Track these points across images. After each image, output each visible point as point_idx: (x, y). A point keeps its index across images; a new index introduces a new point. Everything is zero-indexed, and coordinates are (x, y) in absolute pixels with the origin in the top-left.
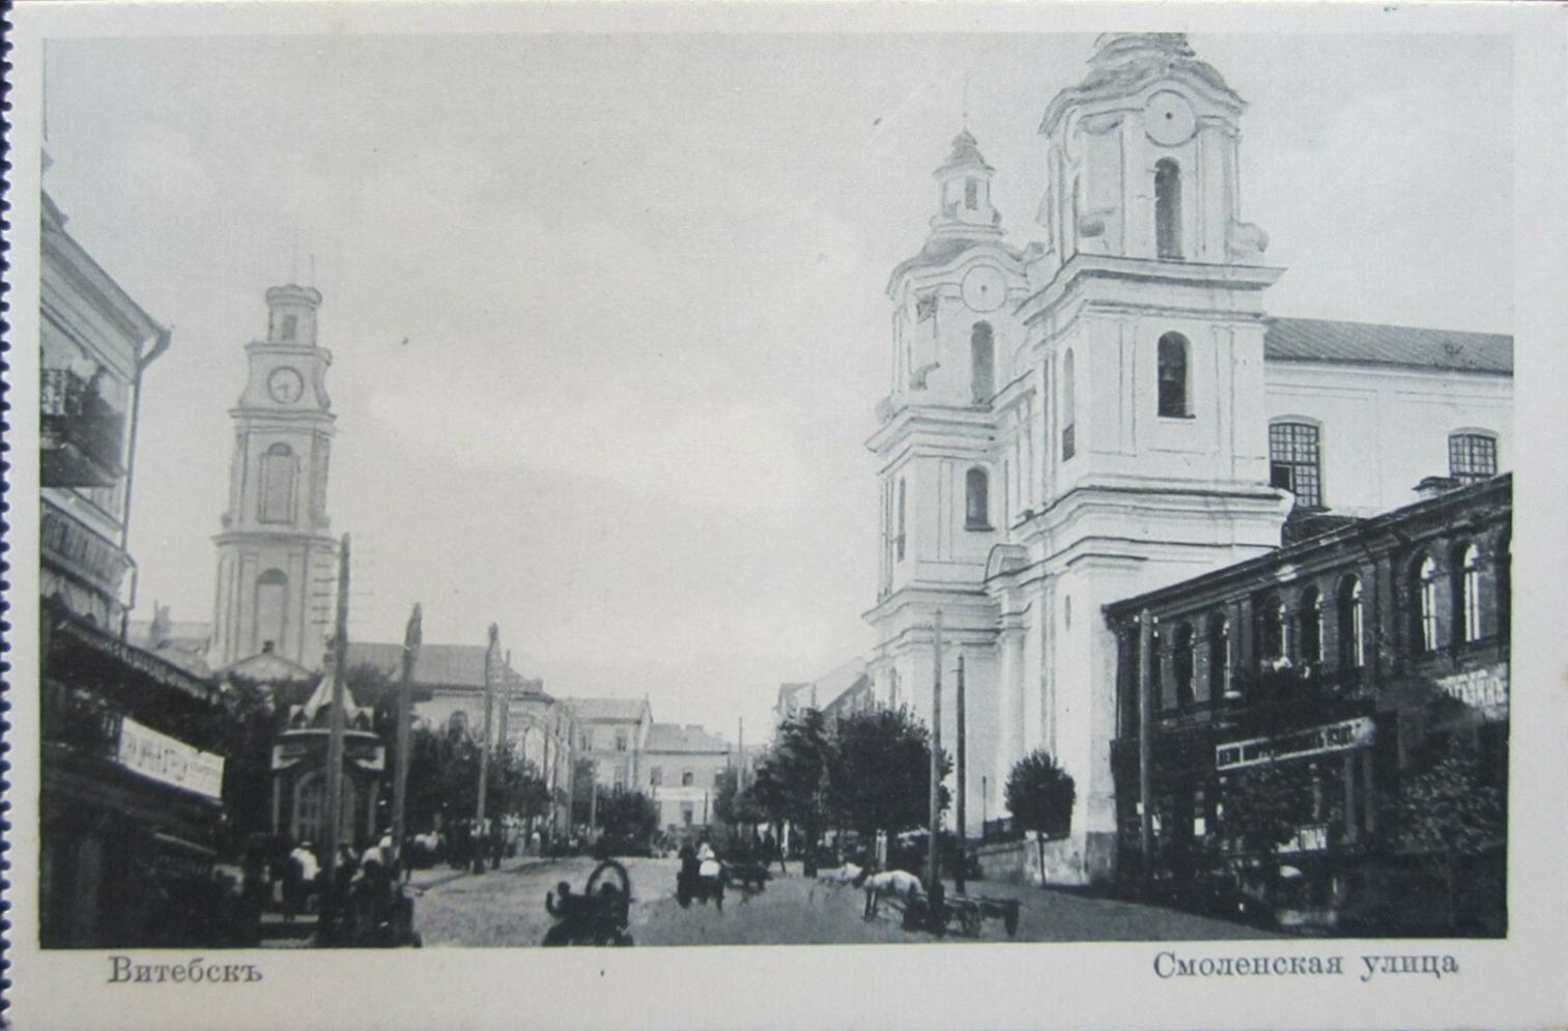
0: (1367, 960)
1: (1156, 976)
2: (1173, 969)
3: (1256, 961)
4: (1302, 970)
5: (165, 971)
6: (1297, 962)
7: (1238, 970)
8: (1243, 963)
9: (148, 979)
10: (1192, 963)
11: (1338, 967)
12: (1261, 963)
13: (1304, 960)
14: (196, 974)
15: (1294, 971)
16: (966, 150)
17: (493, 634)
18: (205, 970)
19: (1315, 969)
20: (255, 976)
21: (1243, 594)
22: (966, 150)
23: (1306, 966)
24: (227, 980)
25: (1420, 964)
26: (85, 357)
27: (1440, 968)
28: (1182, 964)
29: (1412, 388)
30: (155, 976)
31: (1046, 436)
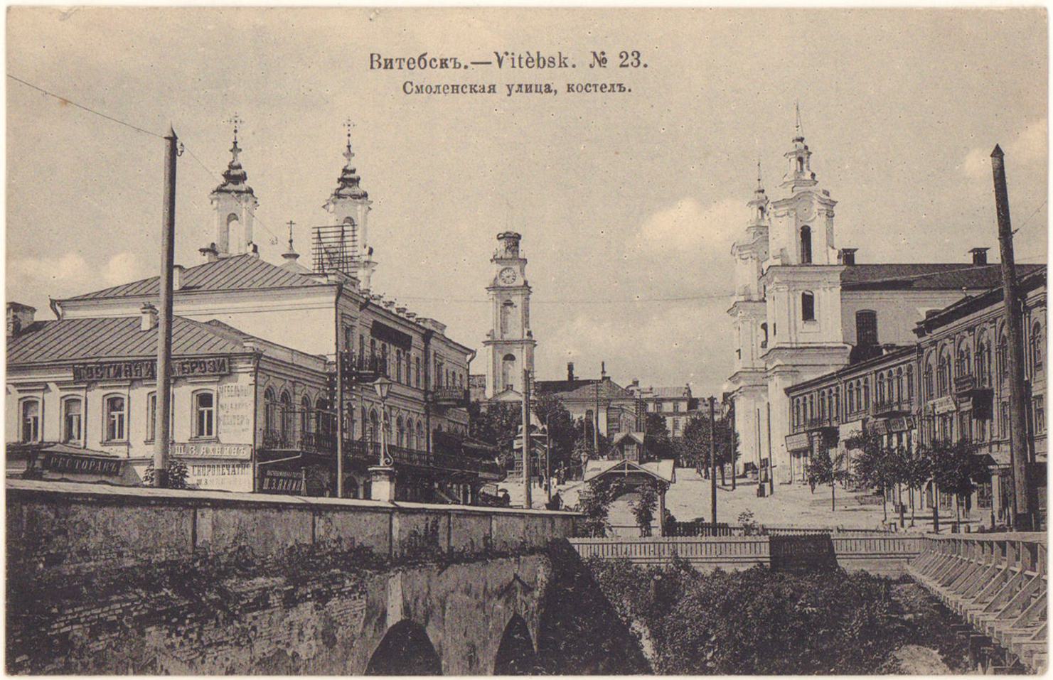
0: (508, 86)
2: (412, 90)
9: (391, 68)
10: (422, 86)
13: (476, 86)
14: (422, 61)
17: (570, 367)
21: (1035, 404)
23: (543, 89)
25: (534, 88)
27: (543, 90)
28: (417, 87)
30: (396, 65)
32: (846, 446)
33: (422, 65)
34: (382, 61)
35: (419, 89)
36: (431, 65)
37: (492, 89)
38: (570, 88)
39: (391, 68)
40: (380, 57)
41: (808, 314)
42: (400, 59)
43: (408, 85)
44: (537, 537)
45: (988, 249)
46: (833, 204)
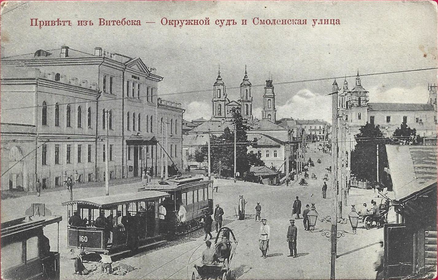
0: (314, 20)
1: (253, 23)
7: (117, 24)
9: (109, 25)
12: (284, 21)
14: (123, 22)
15: (132, 24)
18: (126, 21)
19: (338, 23)
20: (235, 23)
23: (297, 22)
26: (212, 200)
28: (261, 20)
30: (112, 24)
31: (75, 92)
32: (292, 180)
34: (38, 23)
35: (262, 22)
36: (127, 23)
37: (305, 22)
38: (305, 22)
39: (49, 25)
40: (104, 20)
41: (360, 117)
42: (114, 21)
44: (298, 5)
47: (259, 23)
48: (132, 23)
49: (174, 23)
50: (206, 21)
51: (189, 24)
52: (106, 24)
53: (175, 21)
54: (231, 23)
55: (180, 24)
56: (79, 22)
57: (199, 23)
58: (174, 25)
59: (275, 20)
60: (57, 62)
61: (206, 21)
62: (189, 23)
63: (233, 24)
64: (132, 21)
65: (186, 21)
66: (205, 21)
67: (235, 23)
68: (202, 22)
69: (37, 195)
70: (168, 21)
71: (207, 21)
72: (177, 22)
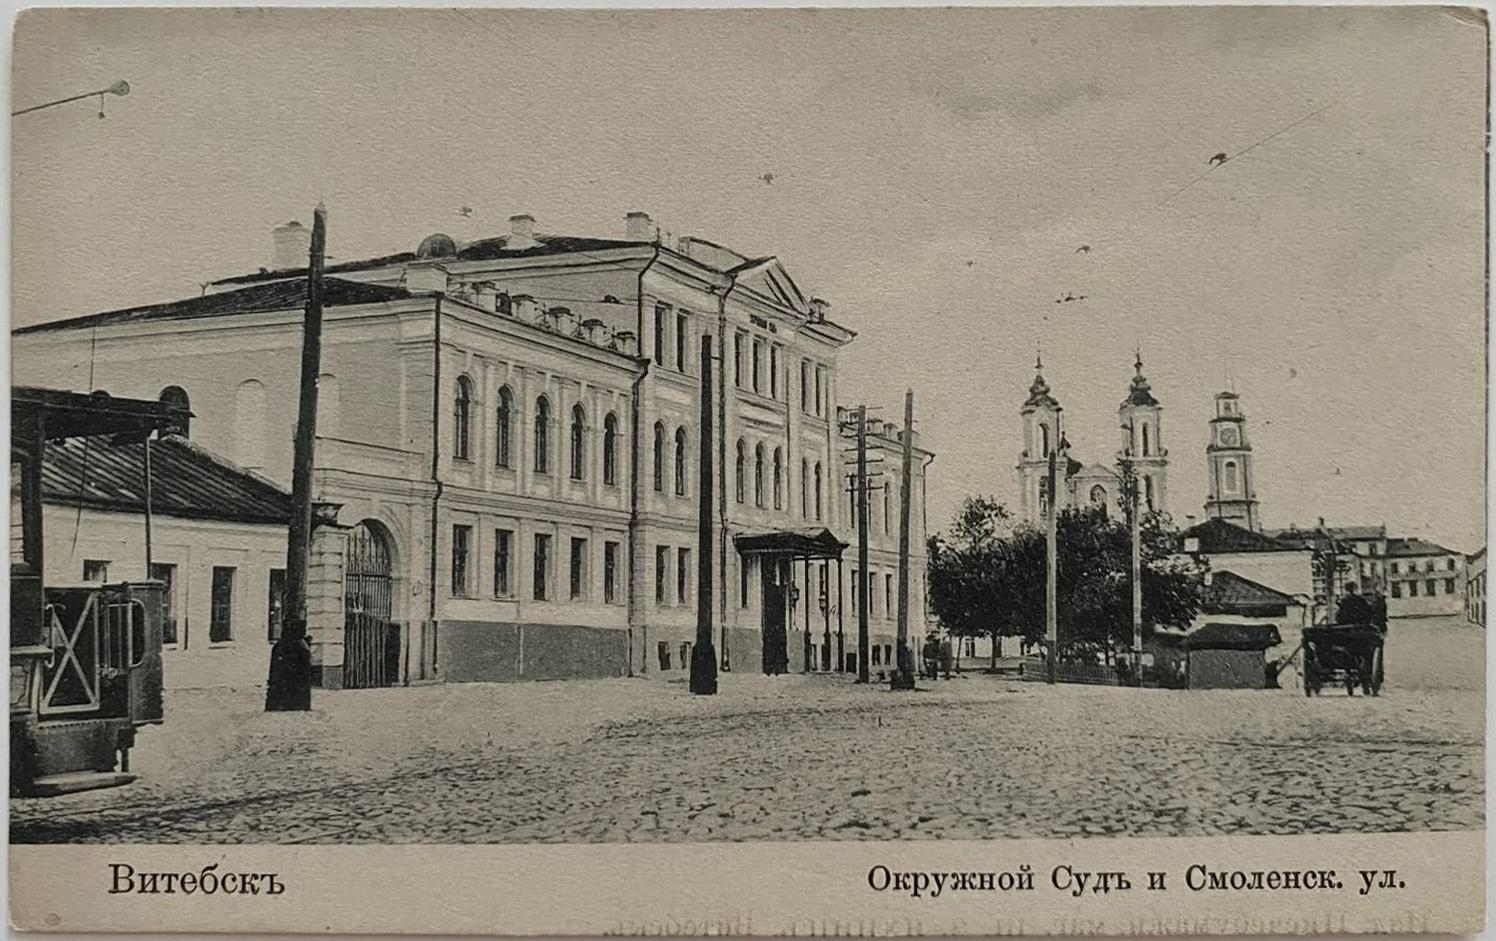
0: (1364, 874)
1: (871, 889)
3: (1287, 874)
4: (972, 887)
5: (173, 879)
6: (248, 879)
7: (1270, 885)
8: (1274, 876)
9: (154, 890)
10: (1223, 875)
11: (1162, 884)
14: (209, 884)
15: (1323, 886)
16: (1039, 395)
22: (1039, 395)
24: (243, 891)
28: (1213, 875)
29: (474, 569)
30: (162, 885)
33: (209, 888)
34: (136, 879)
35: (1219, 881)
39: (154, 890)
40: (131, 871)
42: (170, 876)
43: (1196, 873)
45: (108, 562)
46: (1140, 364)
47: (1208, 884)
48: (244, 883)
49: (910, 882)
50: (1020, 876)
51: (964, 887)
52: (138, 886)
53: (916, 877)
54: (1113, 883)
55: (933, 886)
56: (1162, 884)
57: (1301, 883)
58: (912, 890)
59: (1260, 874)
60: (61, 473)
61: (1020, 876)
62: (963, 882)
63: (271, 891)
64: (1322, 874)
65: (954, 876)
66: (1016, 878)
67: (1124, 885)
68: (1006, 881)
69: (1215, 575)
70: (893, 878)
71: (1025, 877)
72: (921, 882)
